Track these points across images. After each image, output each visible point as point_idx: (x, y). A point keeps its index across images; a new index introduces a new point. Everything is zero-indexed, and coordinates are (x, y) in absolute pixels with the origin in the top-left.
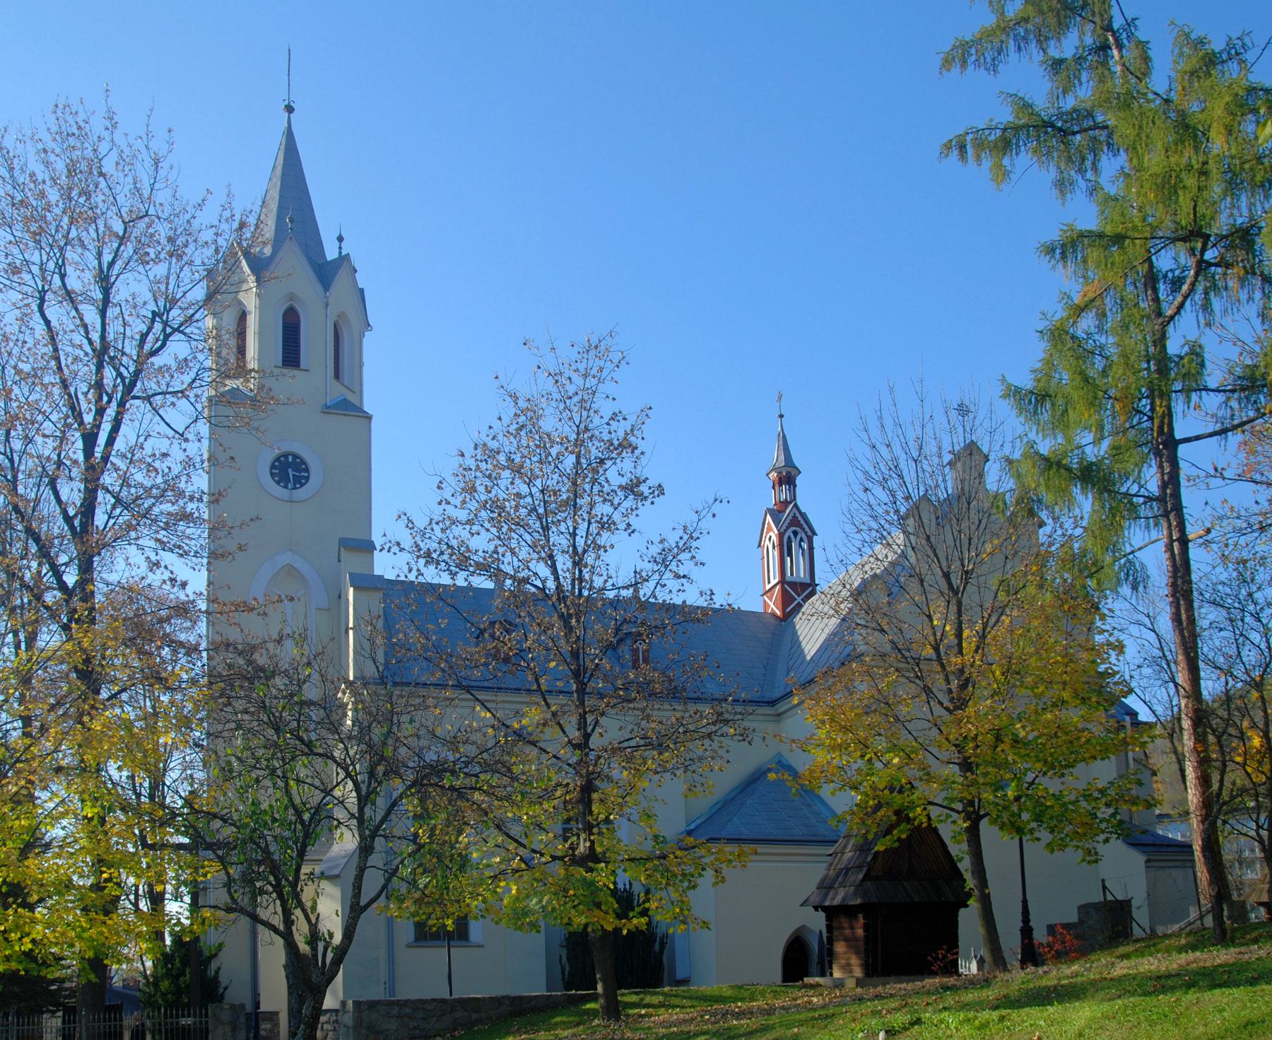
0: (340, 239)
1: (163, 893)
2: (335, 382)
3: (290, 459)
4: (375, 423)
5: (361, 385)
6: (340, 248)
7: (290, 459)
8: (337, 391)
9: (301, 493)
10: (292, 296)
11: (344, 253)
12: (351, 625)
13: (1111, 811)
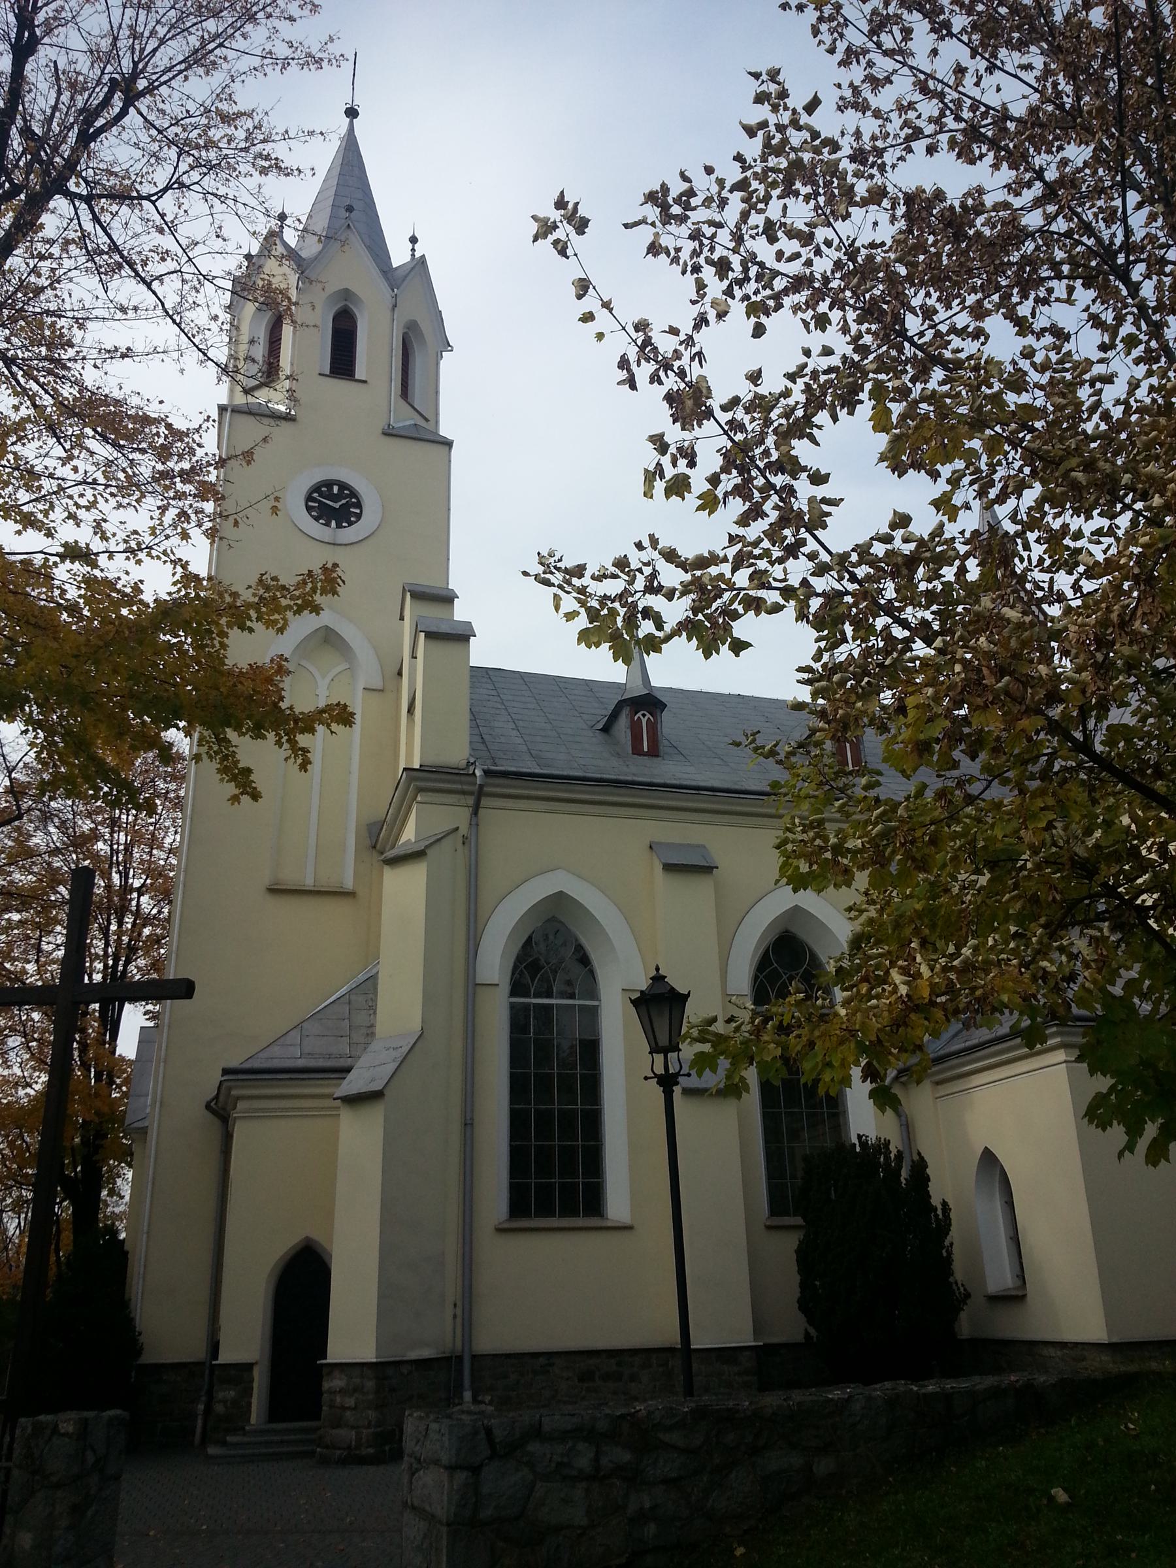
0: (414, 240)
1: (865, 99)
2: (402, 402)
3: (335, 489)
4: (457, 454)
5: (437, 414)
6: (413, 250)
7: (335, 489)
8: (404, 418)
9: (349, 533)
10: (346, 294)
11: (417, 255)
12: (200, 1417)
13: (793, 759)
